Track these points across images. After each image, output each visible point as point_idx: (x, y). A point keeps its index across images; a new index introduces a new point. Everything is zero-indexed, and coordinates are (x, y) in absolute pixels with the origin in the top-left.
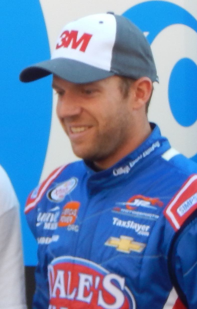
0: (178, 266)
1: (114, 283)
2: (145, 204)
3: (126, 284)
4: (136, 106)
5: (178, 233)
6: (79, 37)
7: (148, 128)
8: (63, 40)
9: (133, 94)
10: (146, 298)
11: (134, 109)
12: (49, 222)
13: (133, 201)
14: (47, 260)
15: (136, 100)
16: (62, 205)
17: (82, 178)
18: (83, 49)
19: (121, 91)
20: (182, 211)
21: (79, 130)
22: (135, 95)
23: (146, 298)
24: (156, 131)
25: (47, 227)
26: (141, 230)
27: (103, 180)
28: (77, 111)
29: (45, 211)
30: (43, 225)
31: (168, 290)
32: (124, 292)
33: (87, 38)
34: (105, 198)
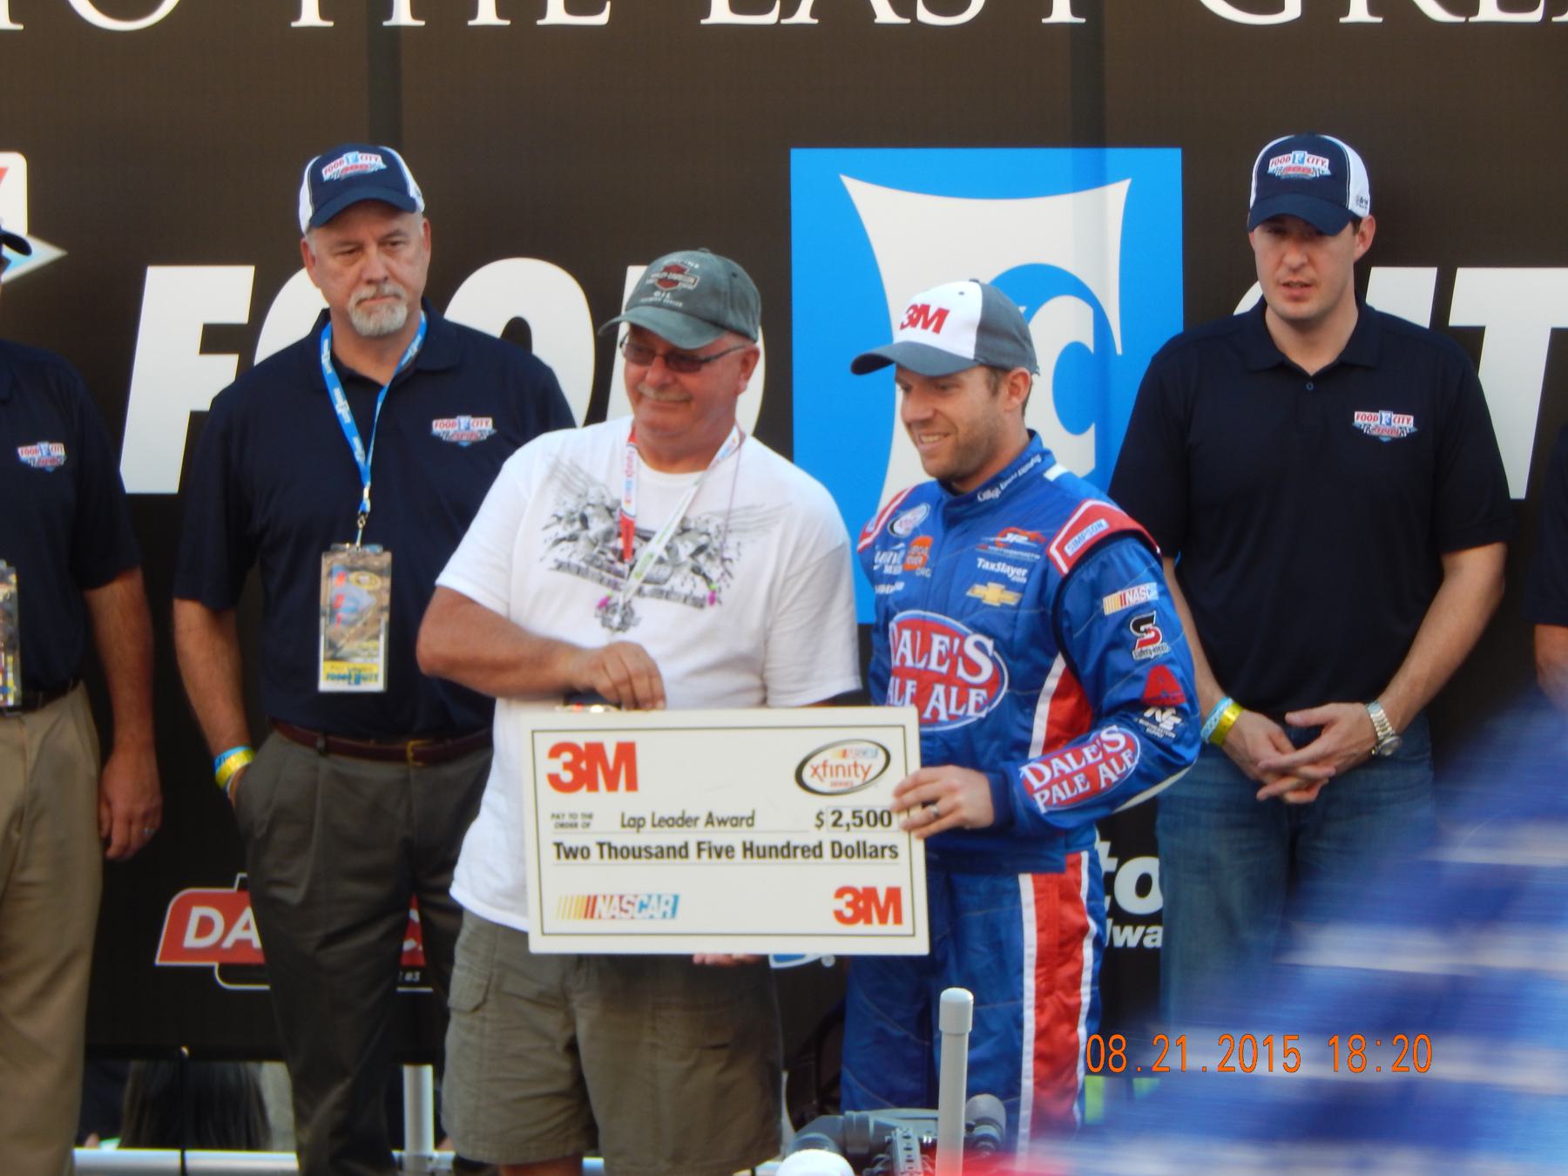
0: (1066, 624)
1: (980, 646)
2: (1021, 539)
3: (996, 648)
4: (1008, 407)
5: (1066, 579)
6: (932, 312)
9: (1004, 390)
11: (1006, 411)
12: (890, 563)
13: (1005, 536)
14: (888, 616)
16: (909, 541)
17: (935, 505)
18: (937, 329)
19: (989, 387)
20: (1072, 549)
21: (931, 439)
22: (1007, 393)
23: (1021, 667)
24: (1035, 440)
25: (888, 570)
26: (1015, 574)
27: (964, 507)
28: (928, 414)
29: (885, 548)
30: (882, 568)
31: (1053, 656)
32: (993, 659)
33: (942, 314)
34: (966, 531)
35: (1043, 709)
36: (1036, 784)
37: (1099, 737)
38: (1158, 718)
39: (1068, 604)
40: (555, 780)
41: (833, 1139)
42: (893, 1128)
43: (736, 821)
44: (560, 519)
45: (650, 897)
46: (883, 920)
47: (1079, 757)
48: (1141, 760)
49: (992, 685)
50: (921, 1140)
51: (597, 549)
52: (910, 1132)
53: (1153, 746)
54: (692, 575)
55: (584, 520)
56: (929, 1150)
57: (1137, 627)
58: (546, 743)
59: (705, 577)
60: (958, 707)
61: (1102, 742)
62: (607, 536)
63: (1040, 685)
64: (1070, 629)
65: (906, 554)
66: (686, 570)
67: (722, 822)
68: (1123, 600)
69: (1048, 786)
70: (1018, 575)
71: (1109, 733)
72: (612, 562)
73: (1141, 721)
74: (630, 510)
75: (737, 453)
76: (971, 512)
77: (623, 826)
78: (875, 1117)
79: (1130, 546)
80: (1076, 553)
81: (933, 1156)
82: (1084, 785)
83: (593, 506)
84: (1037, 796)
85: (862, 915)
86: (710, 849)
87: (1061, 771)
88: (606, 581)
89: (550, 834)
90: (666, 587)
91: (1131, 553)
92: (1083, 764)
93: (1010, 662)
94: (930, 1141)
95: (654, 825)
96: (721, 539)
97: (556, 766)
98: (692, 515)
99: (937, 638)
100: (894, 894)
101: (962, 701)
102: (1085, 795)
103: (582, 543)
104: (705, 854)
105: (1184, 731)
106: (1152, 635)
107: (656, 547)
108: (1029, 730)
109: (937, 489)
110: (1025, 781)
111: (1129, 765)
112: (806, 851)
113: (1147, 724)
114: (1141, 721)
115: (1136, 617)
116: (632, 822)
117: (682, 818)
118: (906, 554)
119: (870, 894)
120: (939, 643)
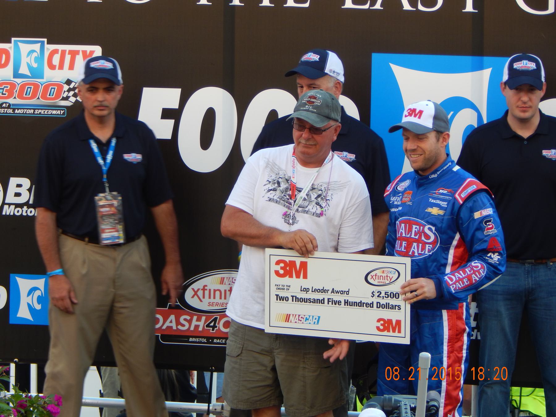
0: (460, 222)
1: (430, 229)
2: (445, 192)
3: (436, 230)
4: (442, 146)
5: (462, 205)
6: (417, 112)
7: (446, 156)
8: (409, 113)
9: (441, 140)
10: (444, 237)
11: (441, 147)
12: (396, 201)
13: (439, 191)
14: (396, 219)
15: (442, 143)
16: (403, 192)
17: (413, 180)
18: (419, 117)
19: (436, 138)
20: (463, 195)
21: (415, 156)
22: (442, 141)
23: (444, 237)
24: (449, 157)
25: (395, 203)
26: (443, 204)
27: (425, 180)
28: (416, 147)
29: (394, 196)
30: (394, 202)
31: (456, 233)
32: (434, 234)
33: (421, 112)
34: (425, 189)
35: (452, 252)
36: (451, 283)
37: (471, 265)
38: (492, 257)
39: (462, 215)
40: (277, 273)
41: (380, 405)
42: (401, 401)
43: (342, 292)
44: (270, 182)
45: (310, 316)
46: (394, 331)
47: (465, 272)
48: (487, 272)
49: (434, 243)
50: (410, 406)
51: (283, 194)
52: (407, 403)
53: (490, 267)
54: (316, 205)
55: (279, 183)
56: (413, 410)
57: (486, 223)
58: (274, 259)
59: (320, 206)
60: (422, 251)
61: (472, 266)
62: (286, 189)
63: (451, 243)
64: (462, 224)
65: (402, 197)
66: (314, 203)
67: (337, 292)
68: (481, 213)
69: (455, 283)
70: (444, 204)
71: (475, 263)
72: (288, 199)
73: (486, 258)
74: (294, 180)
75: (332, 161)
76: (426, 183)
77: (301, 291)
78: (395, 397)
79: (484, 195)
80: (465, 196)
81: (415, 412)
82: (467, 282)
83: (281, 178)
84: (451, 287)
85: (386, 329)
86: (332, 301)
87: (459, 277)
88: (286, 206)
89: (274, 292)
90: (307, 209)
91: (484, 198)
92: (466, 274)
93: (441, 235)
94: (414, 406)
95: (312, 291)
96: (326, 193)
97: (278, 268)
98: (315, 183)
99: (414, 226)
100: (398, 322)
101: (423, 248)
102: (468, 285)
103: (278, 192)
104: (330, 303)
105: (502, 260)
106: (491, 226)
107: (303, 194)
108: (447, 259)
109: (414, 175)
110: (446, 281)
111: (483, 274)
112: (367, 305)
113: (488, 259)
114: (486, 258)
115: (486, 219)
116: (304, 290)
117: (323, 290)
118: (402, 197)
119: (390, 321)
120: (415, 228)
